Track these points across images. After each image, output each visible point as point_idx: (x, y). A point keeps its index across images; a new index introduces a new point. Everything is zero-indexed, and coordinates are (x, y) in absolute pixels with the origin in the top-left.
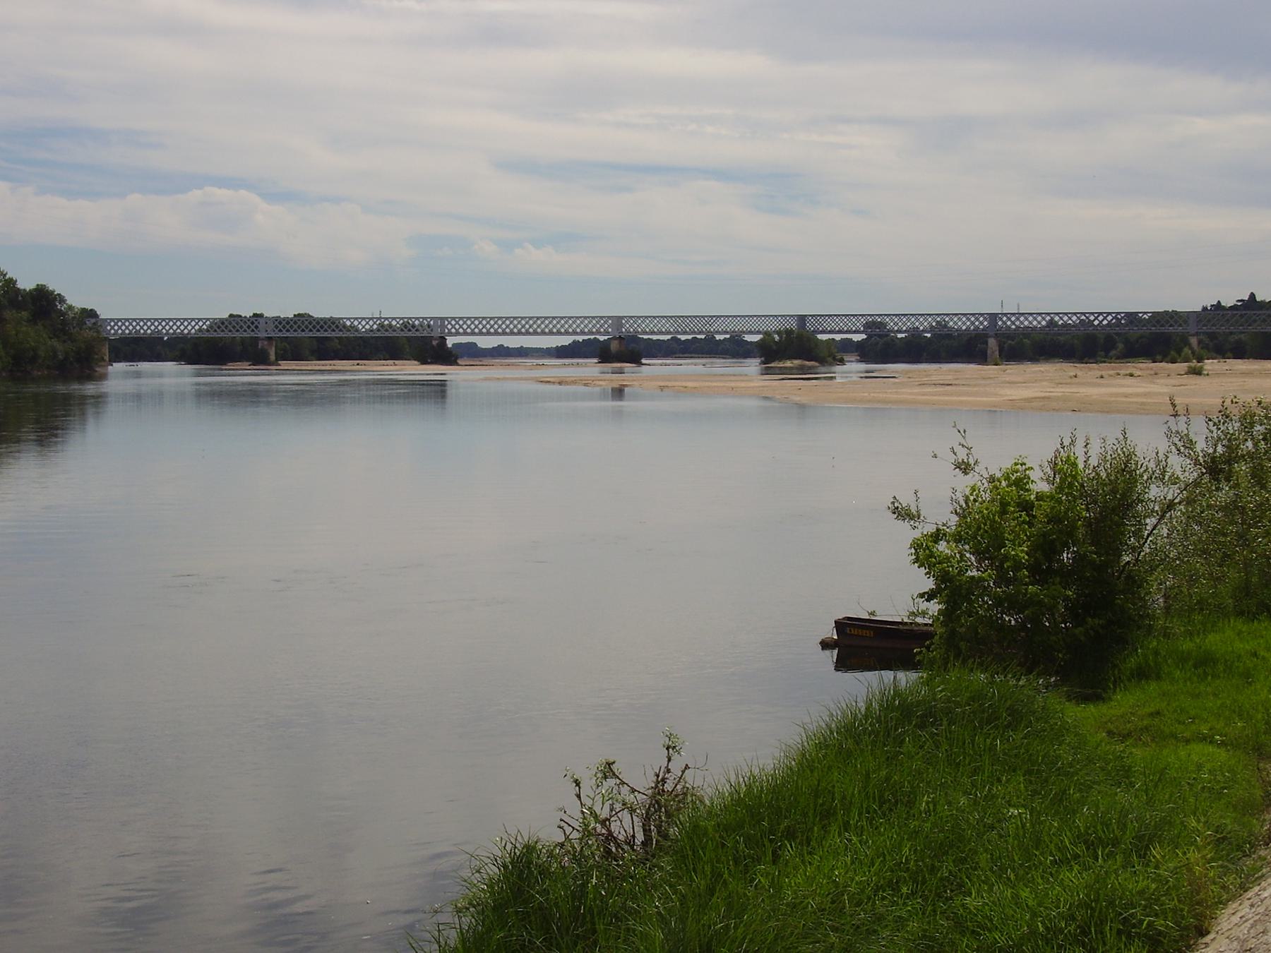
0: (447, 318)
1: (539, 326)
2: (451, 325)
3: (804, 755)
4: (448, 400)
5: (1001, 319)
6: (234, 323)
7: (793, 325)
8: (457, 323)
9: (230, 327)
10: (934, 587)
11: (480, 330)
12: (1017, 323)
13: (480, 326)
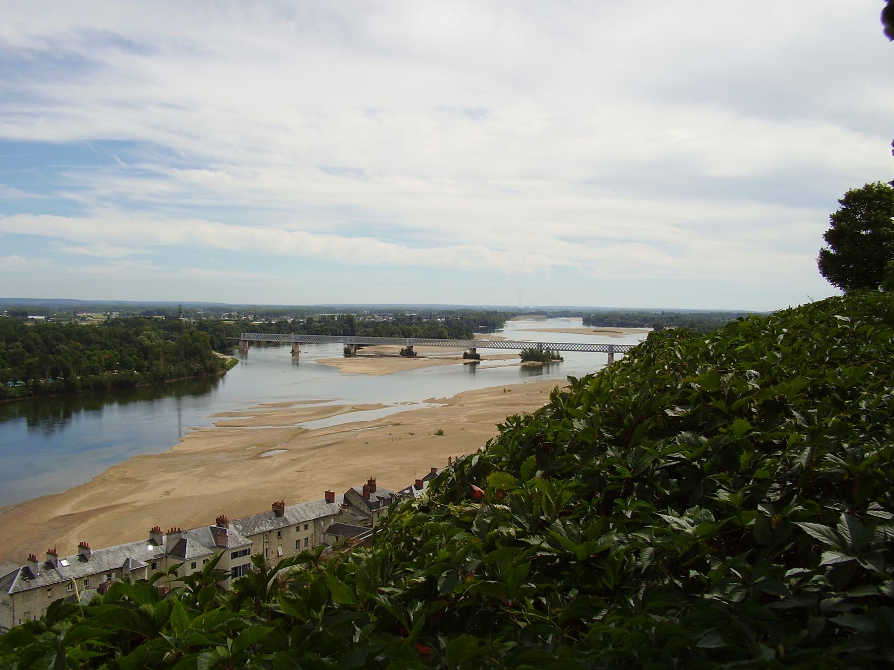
7: (535, 347)
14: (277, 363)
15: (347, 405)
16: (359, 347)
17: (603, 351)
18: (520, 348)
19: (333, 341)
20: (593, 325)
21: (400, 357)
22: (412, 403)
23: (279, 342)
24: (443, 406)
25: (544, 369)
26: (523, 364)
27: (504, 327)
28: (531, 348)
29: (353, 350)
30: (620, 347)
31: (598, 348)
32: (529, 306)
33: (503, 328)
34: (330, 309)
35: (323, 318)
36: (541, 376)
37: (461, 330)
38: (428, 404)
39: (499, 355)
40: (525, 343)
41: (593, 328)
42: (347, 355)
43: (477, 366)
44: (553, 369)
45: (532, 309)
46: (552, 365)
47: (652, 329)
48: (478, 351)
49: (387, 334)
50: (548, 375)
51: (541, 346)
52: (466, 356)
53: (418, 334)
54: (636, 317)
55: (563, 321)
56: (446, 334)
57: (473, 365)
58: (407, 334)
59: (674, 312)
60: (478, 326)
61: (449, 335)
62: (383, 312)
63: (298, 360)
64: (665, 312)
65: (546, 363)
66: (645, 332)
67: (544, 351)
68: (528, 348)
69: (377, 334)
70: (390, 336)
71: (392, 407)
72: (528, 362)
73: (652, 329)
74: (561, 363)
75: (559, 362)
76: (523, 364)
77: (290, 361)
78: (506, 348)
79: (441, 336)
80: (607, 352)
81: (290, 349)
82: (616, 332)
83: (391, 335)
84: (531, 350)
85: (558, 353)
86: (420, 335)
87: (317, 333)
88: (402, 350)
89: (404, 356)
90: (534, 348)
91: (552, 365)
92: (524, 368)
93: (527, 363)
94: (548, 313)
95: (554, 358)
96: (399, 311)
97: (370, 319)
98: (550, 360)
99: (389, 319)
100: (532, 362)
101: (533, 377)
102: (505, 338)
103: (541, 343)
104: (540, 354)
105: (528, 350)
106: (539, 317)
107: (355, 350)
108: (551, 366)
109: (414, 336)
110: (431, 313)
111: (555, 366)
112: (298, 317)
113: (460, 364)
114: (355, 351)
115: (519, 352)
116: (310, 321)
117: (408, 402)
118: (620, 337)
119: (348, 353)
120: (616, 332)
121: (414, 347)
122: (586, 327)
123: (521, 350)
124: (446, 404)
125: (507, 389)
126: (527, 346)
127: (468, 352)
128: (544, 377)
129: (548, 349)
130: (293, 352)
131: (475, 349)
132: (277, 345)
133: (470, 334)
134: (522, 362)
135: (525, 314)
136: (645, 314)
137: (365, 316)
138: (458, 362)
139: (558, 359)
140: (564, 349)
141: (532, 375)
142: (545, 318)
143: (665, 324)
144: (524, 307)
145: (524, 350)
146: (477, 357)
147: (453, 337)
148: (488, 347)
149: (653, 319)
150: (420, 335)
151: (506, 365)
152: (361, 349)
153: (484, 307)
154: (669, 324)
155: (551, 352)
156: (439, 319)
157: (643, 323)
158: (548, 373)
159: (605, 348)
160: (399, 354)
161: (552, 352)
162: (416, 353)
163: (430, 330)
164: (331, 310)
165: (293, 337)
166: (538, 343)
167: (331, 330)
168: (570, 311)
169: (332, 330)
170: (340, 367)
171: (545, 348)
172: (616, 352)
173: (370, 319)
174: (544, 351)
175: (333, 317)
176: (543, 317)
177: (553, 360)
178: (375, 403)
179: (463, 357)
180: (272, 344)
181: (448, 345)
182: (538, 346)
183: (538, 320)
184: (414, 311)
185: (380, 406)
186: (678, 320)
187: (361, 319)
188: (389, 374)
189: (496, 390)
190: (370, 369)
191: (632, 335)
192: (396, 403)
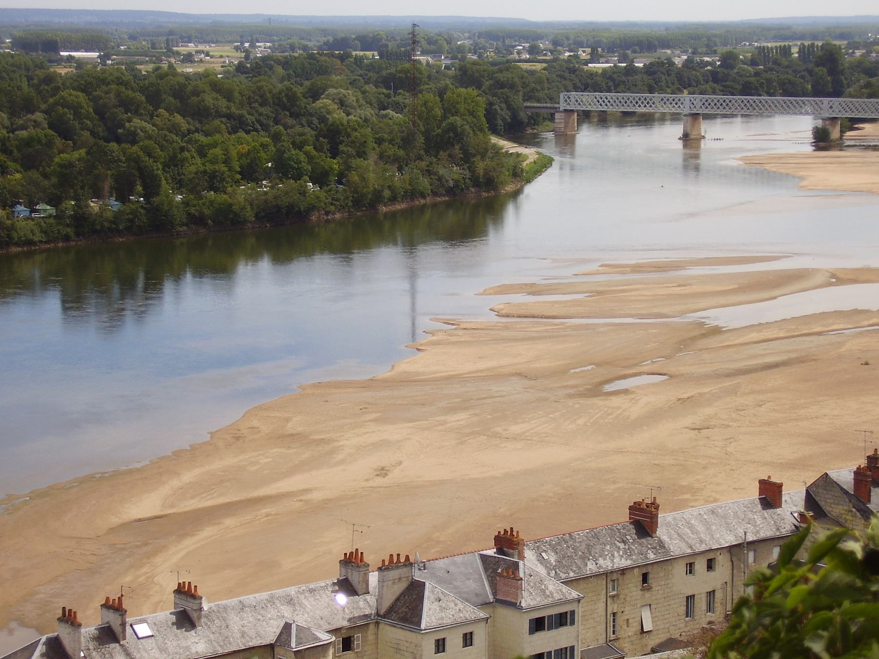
16: (852, 123)
29: (835, 134)
34: (781, 31)
42: (822, 144)
63: (697, 157)
77: (679, 160)
81: (677, 130)
87: (747, 89)
107: (842, 132)
114: (841, 136)
132: (646, 120)
152: (858, 129)
165: (687, 101)
167: (782, 84)
170: (802, 174)
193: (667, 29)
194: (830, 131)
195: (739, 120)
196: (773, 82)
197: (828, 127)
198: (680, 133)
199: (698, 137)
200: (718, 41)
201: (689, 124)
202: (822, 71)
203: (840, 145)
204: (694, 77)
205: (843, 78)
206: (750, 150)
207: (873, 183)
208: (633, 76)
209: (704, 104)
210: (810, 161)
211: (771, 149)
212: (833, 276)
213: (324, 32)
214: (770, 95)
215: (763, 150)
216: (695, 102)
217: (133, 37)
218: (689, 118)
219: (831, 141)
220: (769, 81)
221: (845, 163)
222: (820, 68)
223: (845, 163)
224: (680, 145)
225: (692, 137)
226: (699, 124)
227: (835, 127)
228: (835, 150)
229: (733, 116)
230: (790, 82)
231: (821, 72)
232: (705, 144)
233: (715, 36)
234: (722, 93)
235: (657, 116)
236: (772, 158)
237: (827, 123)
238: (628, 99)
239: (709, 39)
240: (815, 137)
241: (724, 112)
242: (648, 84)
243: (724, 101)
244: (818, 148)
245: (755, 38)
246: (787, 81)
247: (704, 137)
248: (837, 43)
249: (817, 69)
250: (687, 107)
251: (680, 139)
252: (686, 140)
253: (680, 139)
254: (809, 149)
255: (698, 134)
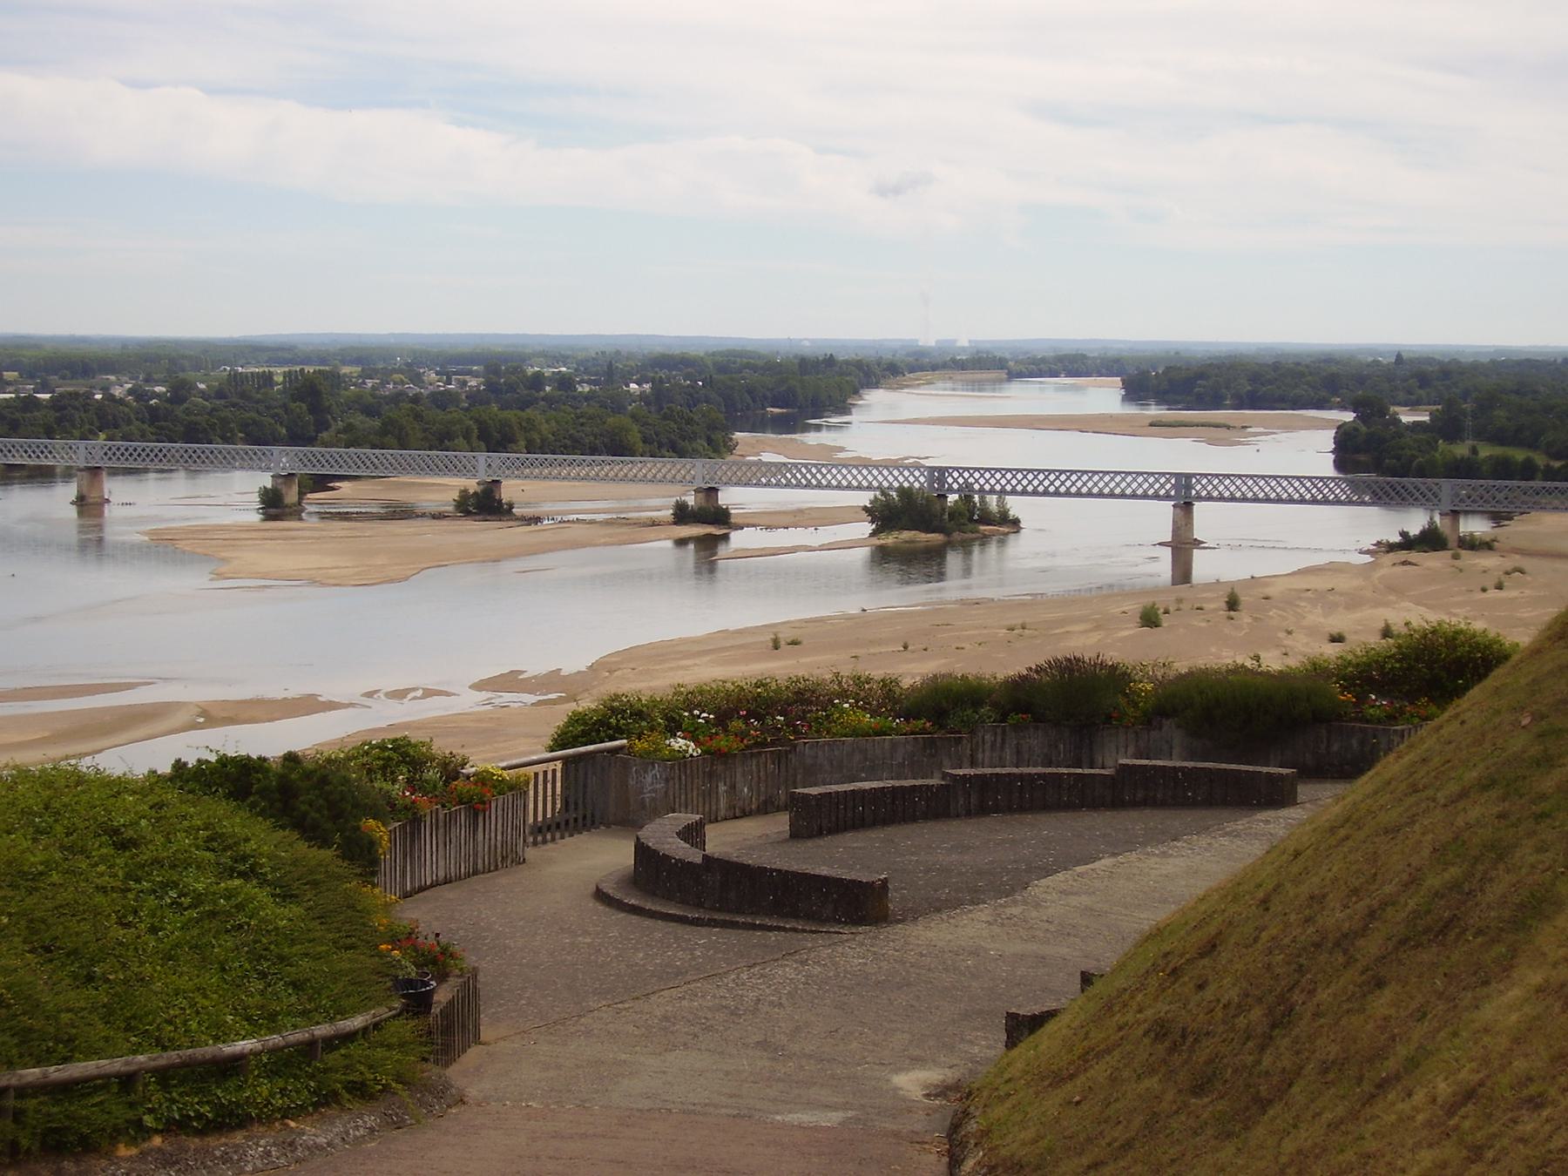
0: (1194, 475)
1: (1052, 483)
2: (914, 476)
3: (1012, 1155)
4: (719, 575)
5: (950, 475)
6: (42, 447)
7: (918, 481)
8: (961, 475)
9: (30, 452)
10: (190, 766)
11: (1014, 487)
12: (961, 480)
13: (1014, 482)
14: (36, 544)
15: (184, 704)
16: (321, 483)
17: (1156, 497)
18: (869, 488)
19: (228, 463)
20: (1158, 404)
21: (454, 518)
22: (429, 693)
23: (52, 468)
24: (540, 703)
25: (953, 560)
26: (876, 541)
27: (854, 410)
28: (906, 485)
29: (291, 496)
30: (1239, 482)
31: (987, 481)
32: (955, 341)
33: (849, 413)
34: (251, 350)
35: (235, 378)
36: (941, 584)
37: (690, 421)
38: (484, 695)
39: (801, 511)
40: (907, 467)
41: (1155, 411)
42: (272, 511)
43: (722, 550)
44: (987, 558)
45: (964, 349)
46: (983, 544)
47: (1349, 417)
48: (729, 497)
49: (425, 439)
50: (965, 582)
51: (942, 480)
52: (682, 515)
53: (536, 436)
54: (1302, 375)
55: (1065, 388)
56: (634, 436)
57: (709, 545)
58: (496, 439)
59: (1437, 357)
60: (764, 408)
61: (645, 441)
62: (452, 361)
63: (100, 527)
64: (1405, 355)
65: (957, 536)
66: (1322, 425)
67: (952, 498)
68: (896, 484)
69: (389, 439)
70: (588, 451)
71: (350, 711)
72: (895, 534)
73: (1349, 417)
74: (1012, 536)
75: (1008, 533)
76: (876, 541)
77: (72, 535)
78: (819, 486)
79: (617, 447)
80: (1167, 497)
81: (69, 491)
82: (1228, 427)
83: (442, 441)
84: (905, 493)
85: (1001, 503)
86: (543, 440)
87: (193, 434)
88: (464, 494)
89: (467, 513)
90: (917, 485)
91: (983, 544)
92: (882, 556)
93: (889, 539)
94: (1011, 364)
95: (986, 519)
96: (504, 358)
97: (403, 383)
98: (971, 526)
99: (465, 383)
100: (906, 535)
101: (910, 589)
102: (842, 449)
103: (1189, 476)
104: (938, 507)
105: (894, 494)
106: (985, 375)
107: (301, 494)
108: (976, 550)
109: (522, 443)
110: (610, 364)
111: (993, 549)
112: (155, 376)
113: (662, 546)
114: (301, 499)
115: (865, 498)
116: (180, 392)
117: (414, 689)
118: (1239, 443)
119: (274, 505)
120: (1228, 427)
121: (504, 483)
122: (1132, 410)
123: (870, 495)
124: (553, 696)
125: (785, 636)
126: (897, 480)
127: (691, 500)
128: (952, 588)
129: (966, 493)
130: (81, 501)
131: (715, 490)
132: (42, 476)
133: (718, 436)
134: (873, 534)
135: (934, 368)
136: (1337, 363)
137: (386, 375)
138: (652, 536)
139: (1000, 524)
140: (1019, 488)
141: (906, 581)
142: (1001, 381)
143: (1401, 396)
144: (937, 342)
145: (883, 493)
146: (721, 517)
147: (660, 446)
148: (778, 485)
149: (1361, 380)
150: (543, 440)
151: (816, 544)
152: (333, 489)
153: (807, 343)
154: (1413, 397)
155: (977, 498)
156: (633, 386)
157: (1323, 393)
158: (967, 572)
159: (1009, 482)
160: (451, 508)
161: (982, 500)
162: (511, 506)
163: (582, 425)
164: (280, 354)
165: (80, 452)
166: (932, 469)
167: (244, 426)
168: (1084, 357)
169: (247, 425)
170: (224, 554)
171: (955, 486)
172: (1199, 498)
173: (403, 383)
174: (952, 498)
175: (267, 379)
176: (993, 375)
177: (982, 528)
178: (290, 695)
179: (671, 519)
180: (25, 473)
181: (611, 474)
182: (931, 480)
183: (979, 386)
184: (563, 356)
185: (308, 705)
186: (1448, 382)
187: (370, 383)
188: (392, 581)
189: (750, 640)
190: (328, 561)
191: (1282, 436)
192: (370, 695)
193: (124, 346)
194: (284, 491)
195: (152, 475)
196: (229, 423)
197: (279, 487)
198: (73, 497)
199: (99, 501)
200: (186, 363)
201: (85, 482)
202: (301, 408)
203: (296, 512)
204: (122, 415)
205: (329, 417)
206: (173, 520)
207: (319, 568)
208: (31, 412)
209: (106, 454)
210: (254, 535)
211: (197, 518)
212: (204, 713)
213: (1027, 353)
214: (226, 440)
215: (188, 519)
216: (93, 452)
217: (628, 359)
218: (84, 473)
219: (286, 506)
220: (224, 421)
221: (293, 538)
222: (298, 403)
223: (293, 538)
224: (72, 512)
225: (91, 501)
226: (101, 482)
227: (290, 487)
228: (293, 520)
229: (146, 471)
230: (255, 422)
231: (298, 409)
232: (110, 511)
233: (184, 357)
234: (154, 438)
235: (58, 470)
236: (193, 532)
237: (280, 481)
238: (203, 452)
239: (172, 361)
240: (262, 502)
241: (160, 466)
242: (44, 424)
243: (177, 451)
244: (269, 517)
245: (243, 361)
246: (251, 422)
247: (108, 501)
248: (345, 370)
249: (293, 405)
250: (82, 458)
251: (72, 503)
252: (82, 505)
253: (72, 503)
254: (255, 518)
255: (99, 497)
